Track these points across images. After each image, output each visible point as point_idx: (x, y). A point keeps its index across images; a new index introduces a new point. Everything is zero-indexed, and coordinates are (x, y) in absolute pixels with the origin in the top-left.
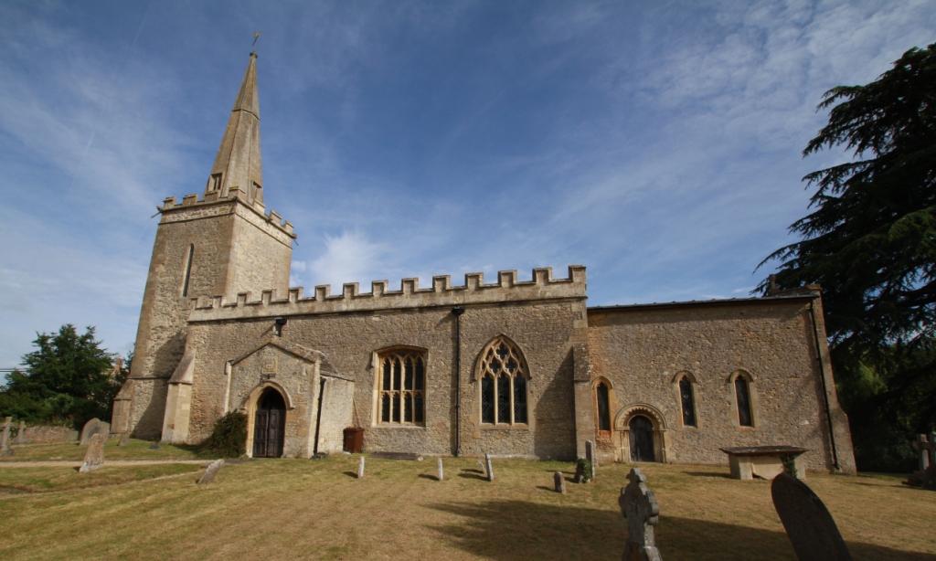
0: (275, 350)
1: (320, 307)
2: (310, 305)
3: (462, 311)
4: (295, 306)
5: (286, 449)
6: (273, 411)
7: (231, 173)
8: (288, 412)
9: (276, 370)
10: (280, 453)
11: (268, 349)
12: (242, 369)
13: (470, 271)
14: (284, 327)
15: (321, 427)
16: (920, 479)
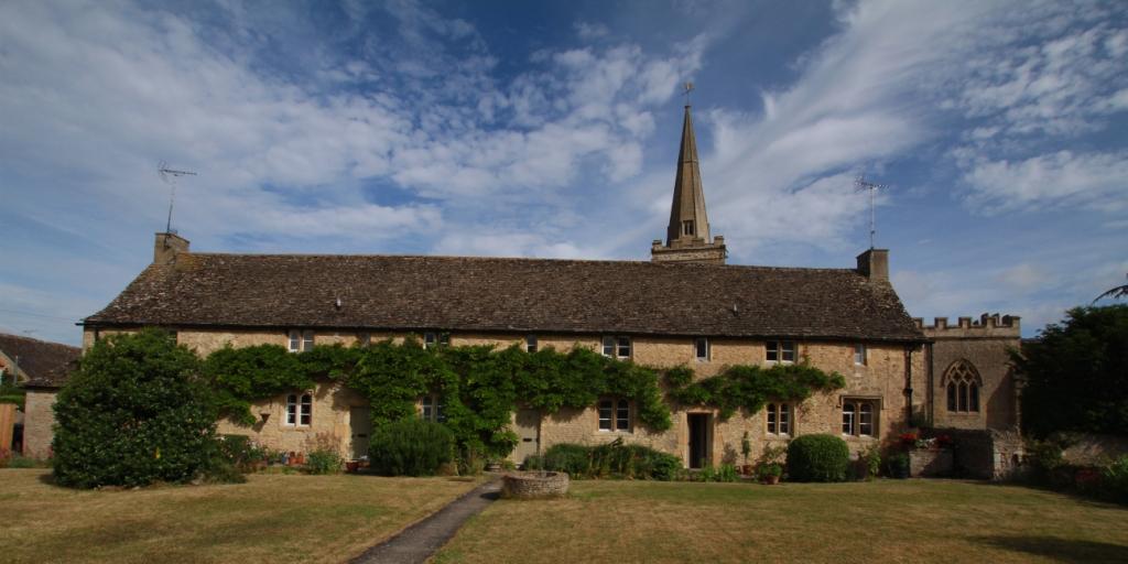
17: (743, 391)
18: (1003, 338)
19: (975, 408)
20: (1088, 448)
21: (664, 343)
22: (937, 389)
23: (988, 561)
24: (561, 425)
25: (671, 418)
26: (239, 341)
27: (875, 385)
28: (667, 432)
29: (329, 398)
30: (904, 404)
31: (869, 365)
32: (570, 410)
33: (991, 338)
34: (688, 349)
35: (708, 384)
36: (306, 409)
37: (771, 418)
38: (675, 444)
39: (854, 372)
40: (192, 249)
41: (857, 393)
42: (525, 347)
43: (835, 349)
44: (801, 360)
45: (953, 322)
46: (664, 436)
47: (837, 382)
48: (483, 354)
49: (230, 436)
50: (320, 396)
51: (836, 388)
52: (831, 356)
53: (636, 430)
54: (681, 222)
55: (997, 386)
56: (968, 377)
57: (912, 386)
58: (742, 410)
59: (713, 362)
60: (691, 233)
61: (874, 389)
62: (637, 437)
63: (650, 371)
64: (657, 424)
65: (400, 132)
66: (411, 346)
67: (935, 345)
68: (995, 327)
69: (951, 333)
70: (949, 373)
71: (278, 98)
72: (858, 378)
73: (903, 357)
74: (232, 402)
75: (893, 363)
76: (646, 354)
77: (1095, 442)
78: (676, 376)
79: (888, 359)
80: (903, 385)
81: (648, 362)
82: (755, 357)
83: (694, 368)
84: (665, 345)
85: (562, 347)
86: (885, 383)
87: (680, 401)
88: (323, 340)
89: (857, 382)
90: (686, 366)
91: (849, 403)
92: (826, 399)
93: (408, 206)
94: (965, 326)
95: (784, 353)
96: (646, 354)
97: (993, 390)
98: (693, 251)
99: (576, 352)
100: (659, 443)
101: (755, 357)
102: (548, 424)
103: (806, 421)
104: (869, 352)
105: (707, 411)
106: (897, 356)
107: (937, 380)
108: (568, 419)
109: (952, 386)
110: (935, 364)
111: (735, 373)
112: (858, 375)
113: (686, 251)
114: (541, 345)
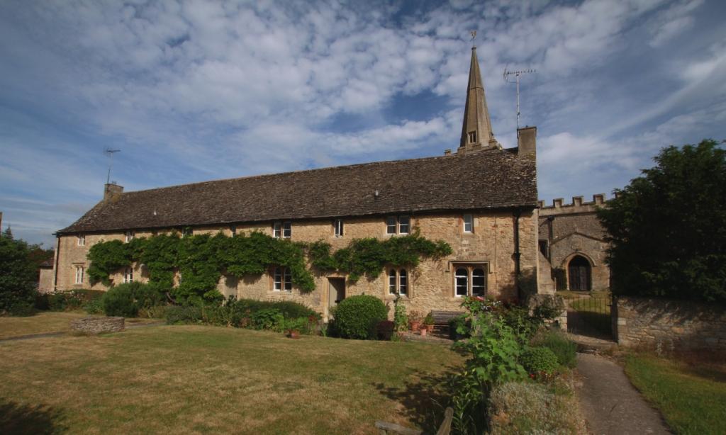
0: (580, 236)
1: (577, 209)
2: (571, 208)
3: (553, 219)
4: (559, 209)
5: (593, 287)
6: (580, 268)
7: (480, 130)
8: (593, 268)
9: (581, 247)
10: (589, 287)
11: (574, 236)
12: (558, 247)
13: (597, 193)
14: (553, 222)
15: (59, 270)
16: (721, 377)
20: (659, 317)
21: (312, 224)
23: (332, 433)
24: (249, 286)
25: (316, 280)
27: (483, 251)
28: (313, 292)
29: (140, 270)
30: (513, 267)
31: (477, 233)
32: (252, 277)
34: (327, 228)
35: (341, 255)
36: (404, 281)
37: (393, 281)
38: (318, 301)
39: (462, 240)
41: (465, 259)
42: (182, 236)
43: (444, 220)
44: (413, 232)
46: (311, 295)
47: (443, 250)
50: (136, 269)
51: (444, 255)
52: (440, 227)
53: (293, 289)
54: (469, 134)
57: (522, 250)
58: (367, 276)
59: (345, 237)
60: (475, 141)
61: (482, 254)
62: (293, 296)
63: (301, 246)
64: (306, 287)
65: (458, 38)
66: (175, 237)
72: (465, 245)
73: (512, 224)
74: (103, 274)
75: (501, 229)
76: (303, 234)
77: (666, 311)
78: (319, 250)
79: (496, 226)
80: (512, 249)
81: (300, 239)
82: (380, 232)
84: (312, 227)
85: (247, 232)
86: (493, 249)
87: (321, 269)
88: (138, 236)
89: (464, 248)
90: (323, 242)
91: (461, 268)
92: (437, 264)
93: (438, 116)
95: (401, 226)
99: (253, 234)
100: (307, 301)
101: (380, 232)
102: (242, 285)
103: (418, 284)
104: (477, 221)
105: (340, 276)
106: (505, 223)
108: (253, 282)
111: (360, 245)
112: (465, 242)
114: (238, 231)
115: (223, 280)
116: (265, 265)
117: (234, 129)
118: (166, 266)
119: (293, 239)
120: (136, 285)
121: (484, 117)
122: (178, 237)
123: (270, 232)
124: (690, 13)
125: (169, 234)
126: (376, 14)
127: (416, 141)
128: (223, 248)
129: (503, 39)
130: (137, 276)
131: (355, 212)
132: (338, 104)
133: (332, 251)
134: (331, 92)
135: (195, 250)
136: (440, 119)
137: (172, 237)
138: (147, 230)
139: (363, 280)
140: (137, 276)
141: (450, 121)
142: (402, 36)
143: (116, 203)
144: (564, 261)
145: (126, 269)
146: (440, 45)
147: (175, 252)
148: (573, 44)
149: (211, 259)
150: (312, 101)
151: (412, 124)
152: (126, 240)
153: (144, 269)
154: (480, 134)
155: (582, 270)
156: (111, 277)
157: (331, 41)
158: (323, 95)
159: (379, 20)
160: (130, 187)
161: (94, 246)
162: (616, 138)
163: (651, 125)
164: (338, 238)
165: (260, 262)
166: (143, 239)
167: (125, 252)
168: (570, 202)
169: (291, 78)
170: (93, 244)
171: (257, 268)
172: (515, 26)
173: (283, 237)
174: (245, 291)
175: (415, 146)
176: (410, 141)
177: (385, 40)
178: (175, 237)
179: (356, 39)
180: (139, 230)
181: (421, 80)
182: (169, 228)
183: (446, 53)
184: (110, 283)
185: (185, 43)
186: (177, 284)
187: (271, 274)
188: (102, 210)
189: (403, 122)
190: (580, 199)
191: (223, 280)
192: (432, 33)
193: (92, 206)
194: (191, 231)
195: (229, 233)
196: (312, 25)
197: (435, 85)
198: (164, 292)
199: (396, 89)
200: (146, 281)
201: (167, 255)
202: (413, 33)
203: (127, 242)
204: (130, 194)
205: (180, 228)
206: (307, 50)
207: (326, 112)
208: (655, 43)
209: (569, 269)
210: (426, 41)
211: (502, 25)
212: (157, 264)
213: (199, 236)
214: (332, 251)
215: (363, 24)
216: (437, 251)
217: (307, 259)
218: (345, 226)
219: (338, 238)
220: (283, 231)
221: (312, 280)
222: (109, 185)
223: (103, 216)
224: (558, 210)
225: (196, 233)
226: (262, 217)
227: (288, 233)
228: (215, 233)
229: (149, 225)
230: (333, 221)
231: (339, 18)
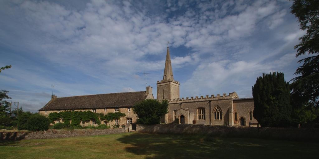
1: (187, 101)
2: (186, 101)
7: (168, 75)
17: (111, 117)
18: (227, 99)
19: (221, 118)
22: (212, 114)
25: (101, 122)
26: (52, 112)
32: (88, 121)
33: (224, 99)
35: (106, 116)
40: (57, 97)
42: (72, 111)
43: (125, 109)
45: (215, 96)
48: (77, 112)
49: (125, 136)
50: (61, 119)
55: (226, 112)
56: (219, 110)
63: (98, 114)
65: (191, 27)
67: (211, 102)
68: (225, 96)
69: (215, 99)
70: (215, 109)
71: (153, 23)
74: (52, 121)
76: (99, 111)
78: (102, 115)
81: (98, 112)
82: (114, 111)
83: (104, 113)
85: (87, 110)
88: (61, 111)
91: (128, 119)
93: (188, 55)
94: (218, 97)
96: (99, 111)
97: (225, 113)
98: (165, 83)
101: (114, 111)
102: (86, 123)
107: (212, 111)
108: (88, 122)
109: (215, 113)
110: (211, 107)
113: (163, 83)
114: (85, 110)
115: (81, 122)
116: (90, 119)
117: (103, 61)
118: (68, 119)
119: (97, 112)
120: (61, 123)
121: (170, 70)
122: (71, 112)
123: (91, 111)
124: (282, 18)
125: (69, 111)
126: (158, 18)
127: (180, 65)
128: (81, 114)
129: (210, 27)
130: (61, 121)
131: (108, 107)
132: (146, 51)
133: (104, 115)
134: (143, 46)
135: (75, 115)
136: (189, 56)
137: (70, 112)
138: (63, 110)
139: (110, 122)
140: (61, 121)
141: (193, 57)
142: (169, 26)
143: (55, 101)
144: (179, 116)
145: (58, 120)
146: (185, 29)
147: (70, 115)
148: (238, 28)
149: (78, 117)
150: (136, 49)
151: (178, 58)
152: (58, 112)
153: (62, 119)
154: (168, 76)
155: (183, 118)
156: (54, 122)
157: (141, 28)
158: (140, 47)
159: (160, 20)
160: (59, 96)
161: (50, 114)
162: (265, 62)
163: (278, 57)
164: (105, 112)
165: (89, 118)
166: (62, 112)
167: (58, 115)
168: (216, 96)
169: (127, 40)
170: (49, 113)
171: (88, 119)
172: (214, 22)
173: (95, 112)
174: (86, 124)
175: (180, 67)
176: (178, 65)
177: (163, 27)
178: (70, 112)
179: (152, 27)
180: (61, 110)
181: (179, 42)
182: (69, 109)
183: (187, 32)
184: (54, 123)
185: (84, 29)
186: (71, 123)
187: (92, 120)
188: (51, 103)
189: (174, 57)
190: (225, 94)
191: (81, 122)
192: (181, 25)
193: (48, 102)
194: (74, 110)
195: (83, 111)
196: (133, 23)
197: (186, 43)
198: (68, 125)
199: (170, 45)
200: (63, 122)
201: (68, 116)
202: (173, 25)
203: (58, 113)
204: (59, 98)
205: (71, 109)
206: (132, 31)
207: (141, 54)
208: (271, 27)
209: (181, 119)
210: (179, 27)
211: (208, 22)
212: (66, 118)
213: (76, 112)
214: (104, 115)
215: (153, 22)
216: (123, 115)
217: (99, 117)
218: (107, 110)
219: (105, 112)
220: (95, 110)
221: (100, 122)
222: (52, 96)
223: (51, 105)
224: (183, 101)
225: (75, 111)
226: (90, 107)
227: (95, 111)
228: (79, 111)
229: (64, 108)
230: (104, 108)
231: (144, 20)
